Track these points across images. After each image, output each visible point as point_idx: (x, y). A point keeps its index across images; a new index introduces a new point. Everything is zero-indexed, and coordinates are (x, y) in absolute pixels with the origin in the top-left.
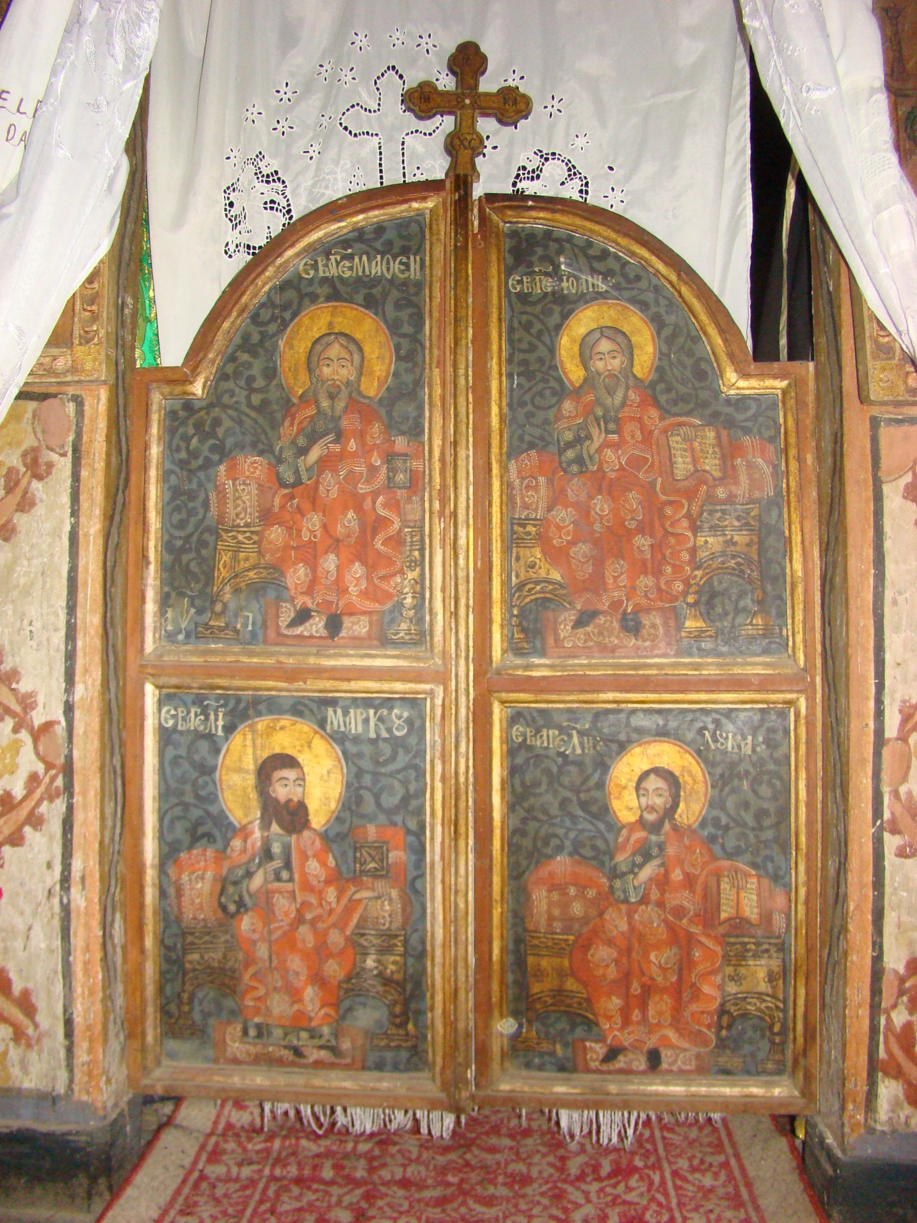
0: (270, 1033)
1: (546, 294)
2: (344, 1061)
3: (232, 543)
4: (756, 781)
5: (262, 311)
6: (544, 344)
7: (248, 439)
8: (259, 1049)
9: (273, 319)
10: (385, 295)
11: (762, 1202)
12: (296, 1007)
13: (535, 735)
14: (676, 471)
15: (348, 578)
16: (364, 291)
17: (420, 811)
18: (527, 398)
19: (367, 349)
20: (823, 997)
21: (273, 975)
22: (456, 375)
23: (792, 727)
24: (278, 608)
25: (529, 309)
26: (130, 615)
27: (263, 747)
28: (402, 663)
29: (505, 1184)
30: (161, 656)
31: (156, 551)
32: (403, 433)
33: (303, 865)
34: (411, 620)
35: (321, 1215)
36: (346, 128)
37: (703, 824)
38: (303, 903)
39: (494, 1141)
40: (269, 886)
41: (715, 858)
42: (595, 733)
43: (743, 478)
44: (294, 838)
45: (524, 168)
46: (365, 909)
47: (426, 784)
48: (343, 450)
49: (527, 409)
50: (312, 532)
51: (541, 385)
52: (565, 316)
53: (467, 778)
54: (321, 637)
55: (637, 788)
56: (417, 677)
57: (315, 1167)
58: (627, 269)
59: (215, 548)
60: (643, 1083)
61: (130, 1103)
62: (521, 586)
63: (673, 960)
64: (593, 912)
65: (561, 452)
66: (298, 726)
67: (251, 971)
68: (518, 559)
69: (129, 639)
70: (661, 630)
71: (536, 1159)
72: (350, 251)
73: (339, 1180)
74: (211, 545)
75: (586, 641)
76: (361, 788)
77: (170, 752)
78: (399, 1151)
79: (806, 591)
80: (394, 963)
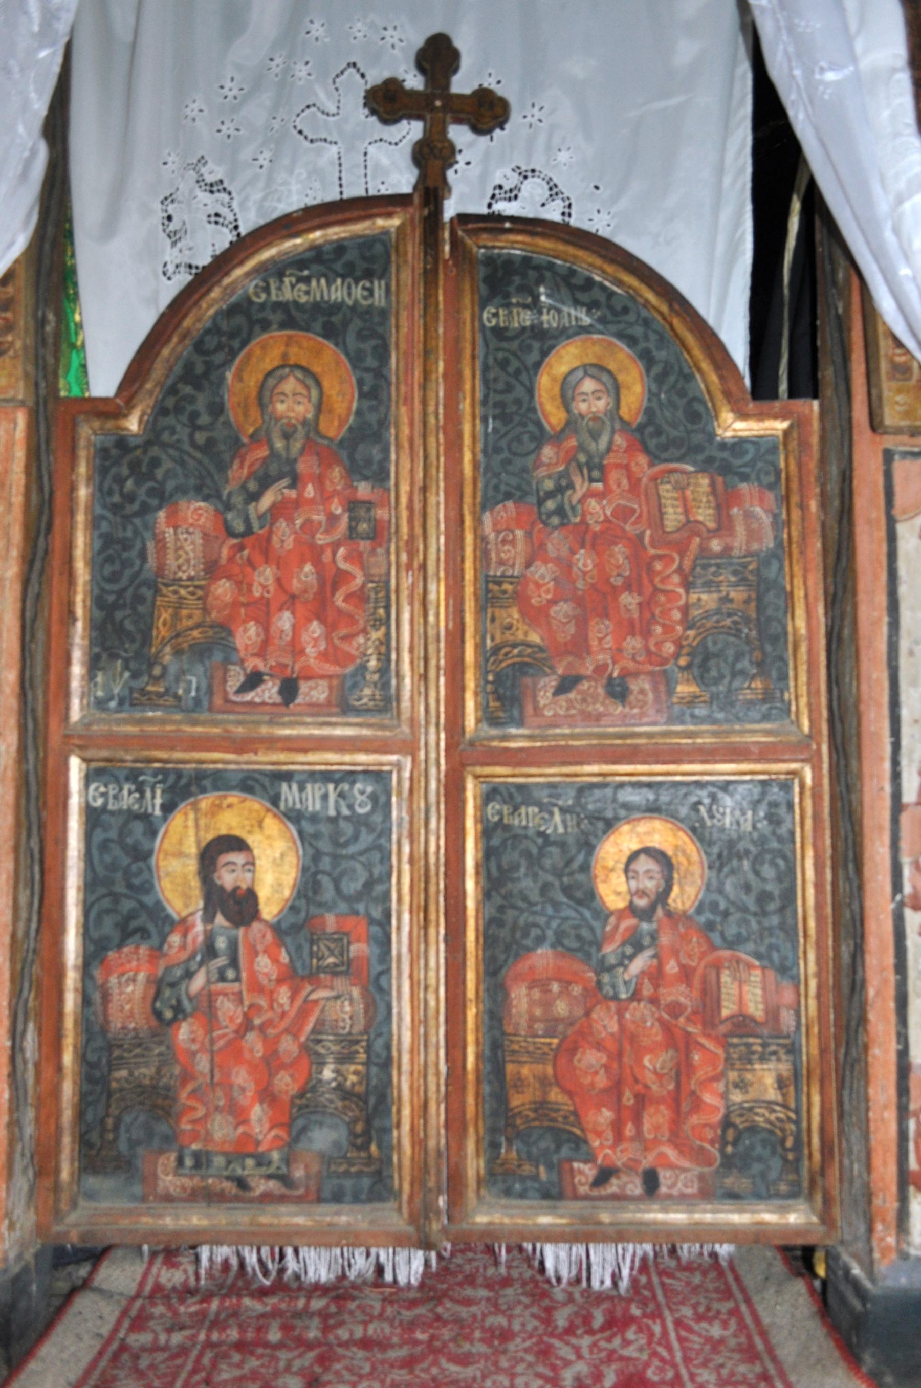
0: (209, 1163)
1: (523, 329)
3: (173, 598)
4: (757, 862)
5: (207, 338)
6: (522, 383)
7: (192, 482)
8: (196, 1181)
9: (219, 347)
10: (346, 323)
11: (781, 1353)
12: (241, 1130)
14: (667, 523)
15: (305, 637)
18: (503, 443)
19: (326, 384)
20: (840, 1103)
21: (214, 1091)
22: (425, 414)
23: (797, 800)
24: (226, 671)
25: (504, 345)
26: (53, 677)
28: (366, 732)
29: (482, 1340)
30: (89, 725)
31: (85, 606)
32: (366, 478)
33: (251, 962)
34: (375, 684)
35: (267, 1382)
36: (300, 132)
37: (700, 910)
38: (251, 1006)
39: (469, 1292)
40: (213, 987)
41: (713, 947)
42: (578, 809)
43: (740, 530)
44: (241, 932)
45: (501, 187)
46: (323, 1011)
47: (391, 867)
48: (300, 495)
50: (264, 587)
51: (519, 429)
52: (545, 353)
53: (438, 859)
54: (274, 704)
55: (626, 870)
56: (383, 747)
57: (259, 1329)
60: (639, 1211)
61: (37, 1256)
62: (496, 650)
63: (669, 1065)
64: (579, 1011)
65: (540, 502)
66: (248, 804)
67: (189, 1087)
68: (493, 620)
69: (51, 707)
70: (651, 696)
71: (518, 1310)
72: (306, 273)
73: (289, 1342)
77: (99, 836)
78: (359, 1307)
79: (810, 651)
80: (356, 1073)
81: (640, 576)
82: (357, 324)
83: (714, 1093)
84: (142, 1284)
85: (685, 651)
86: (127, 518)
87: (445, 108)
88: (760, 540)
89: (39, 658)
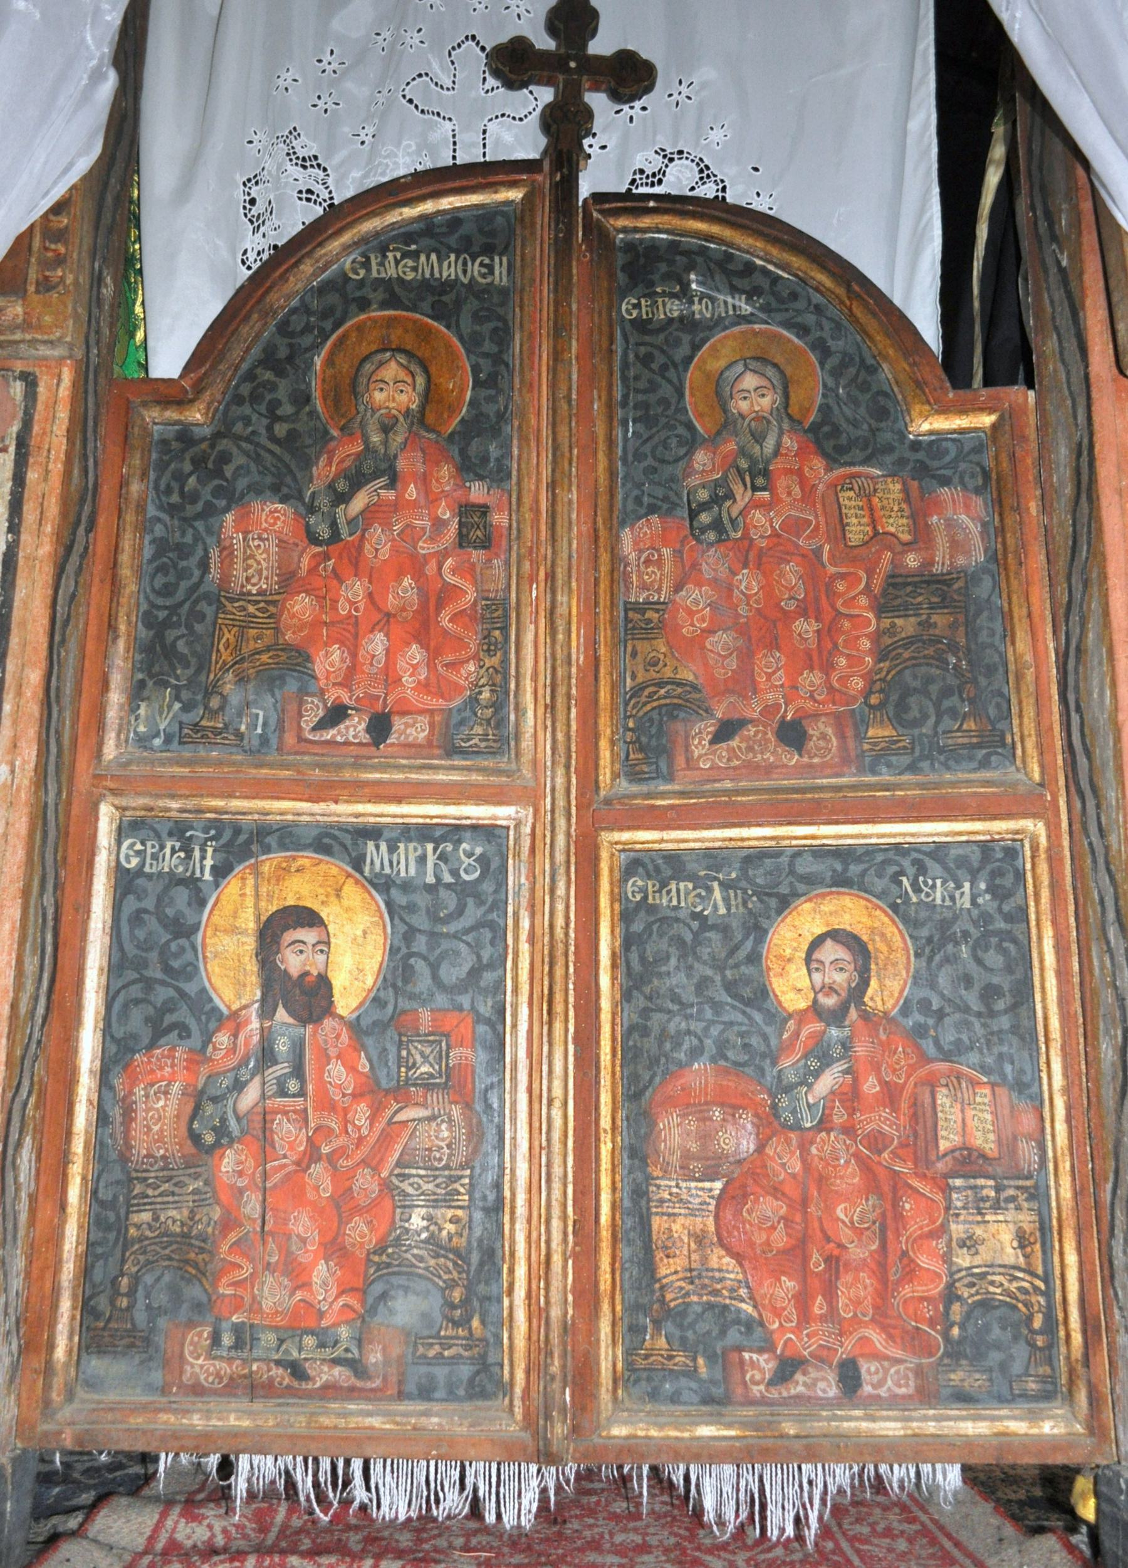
1: (671, 321)
2: (369, 1385)
6: (670, 381)
7: (269, 480)
9: (308, 329)
10: (458, 303)
13: (660, 891)
14: (849, 535)
15: (401, 664)
16: (430, 299)
17: (499, 986)
18: (647, 449)
24: (301, 703)
25: (647, 339)
26: (85, 706)
27: (270, 897)
28: (475, 777)
30: (128, 763)
32: (481, 478)
33: (321, 1070)
36: (410, 101)
37: (905, 1011)
41: (925, 1059)
42: (743, 884)
47: (506, 947)
49: (645, 464)
50: (351, 603)
54: (361, 744)
55: (808, 960)
56: (498, 797)
58: (779, 287)
59: (215, 623)
62: (637, 691)
63: (871, 1216)
65: (693, 515)
66: (323, 867)
67: (233, 1237)
68: (634, 654)
72: (414, 247)
74: (209, 619)
75: (729, 760)
76: (411, 955)
80: (454, 1220)
81: (817, 600)
82: (472, 305)
83: (932, 1254)
84: (152, 1539)
85: (877, 686)
86: (187, 521)
87: (580, 69)
88: (967, 553)
89: (70, 673)
